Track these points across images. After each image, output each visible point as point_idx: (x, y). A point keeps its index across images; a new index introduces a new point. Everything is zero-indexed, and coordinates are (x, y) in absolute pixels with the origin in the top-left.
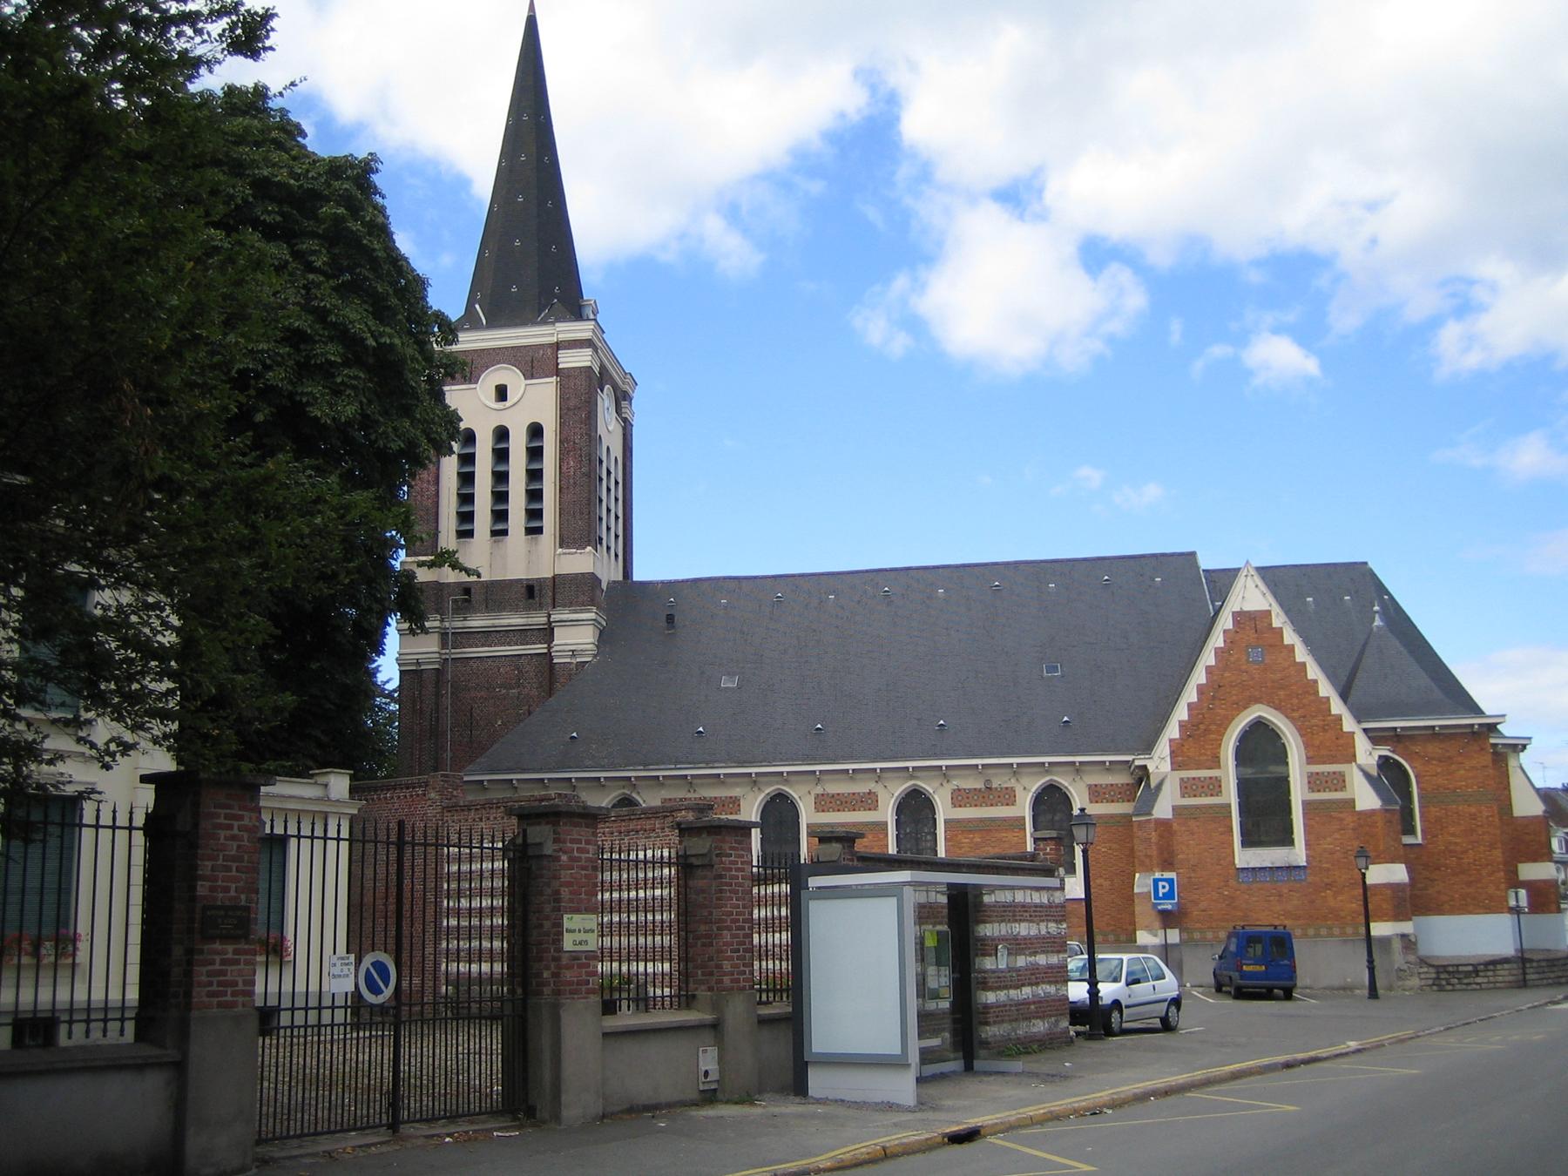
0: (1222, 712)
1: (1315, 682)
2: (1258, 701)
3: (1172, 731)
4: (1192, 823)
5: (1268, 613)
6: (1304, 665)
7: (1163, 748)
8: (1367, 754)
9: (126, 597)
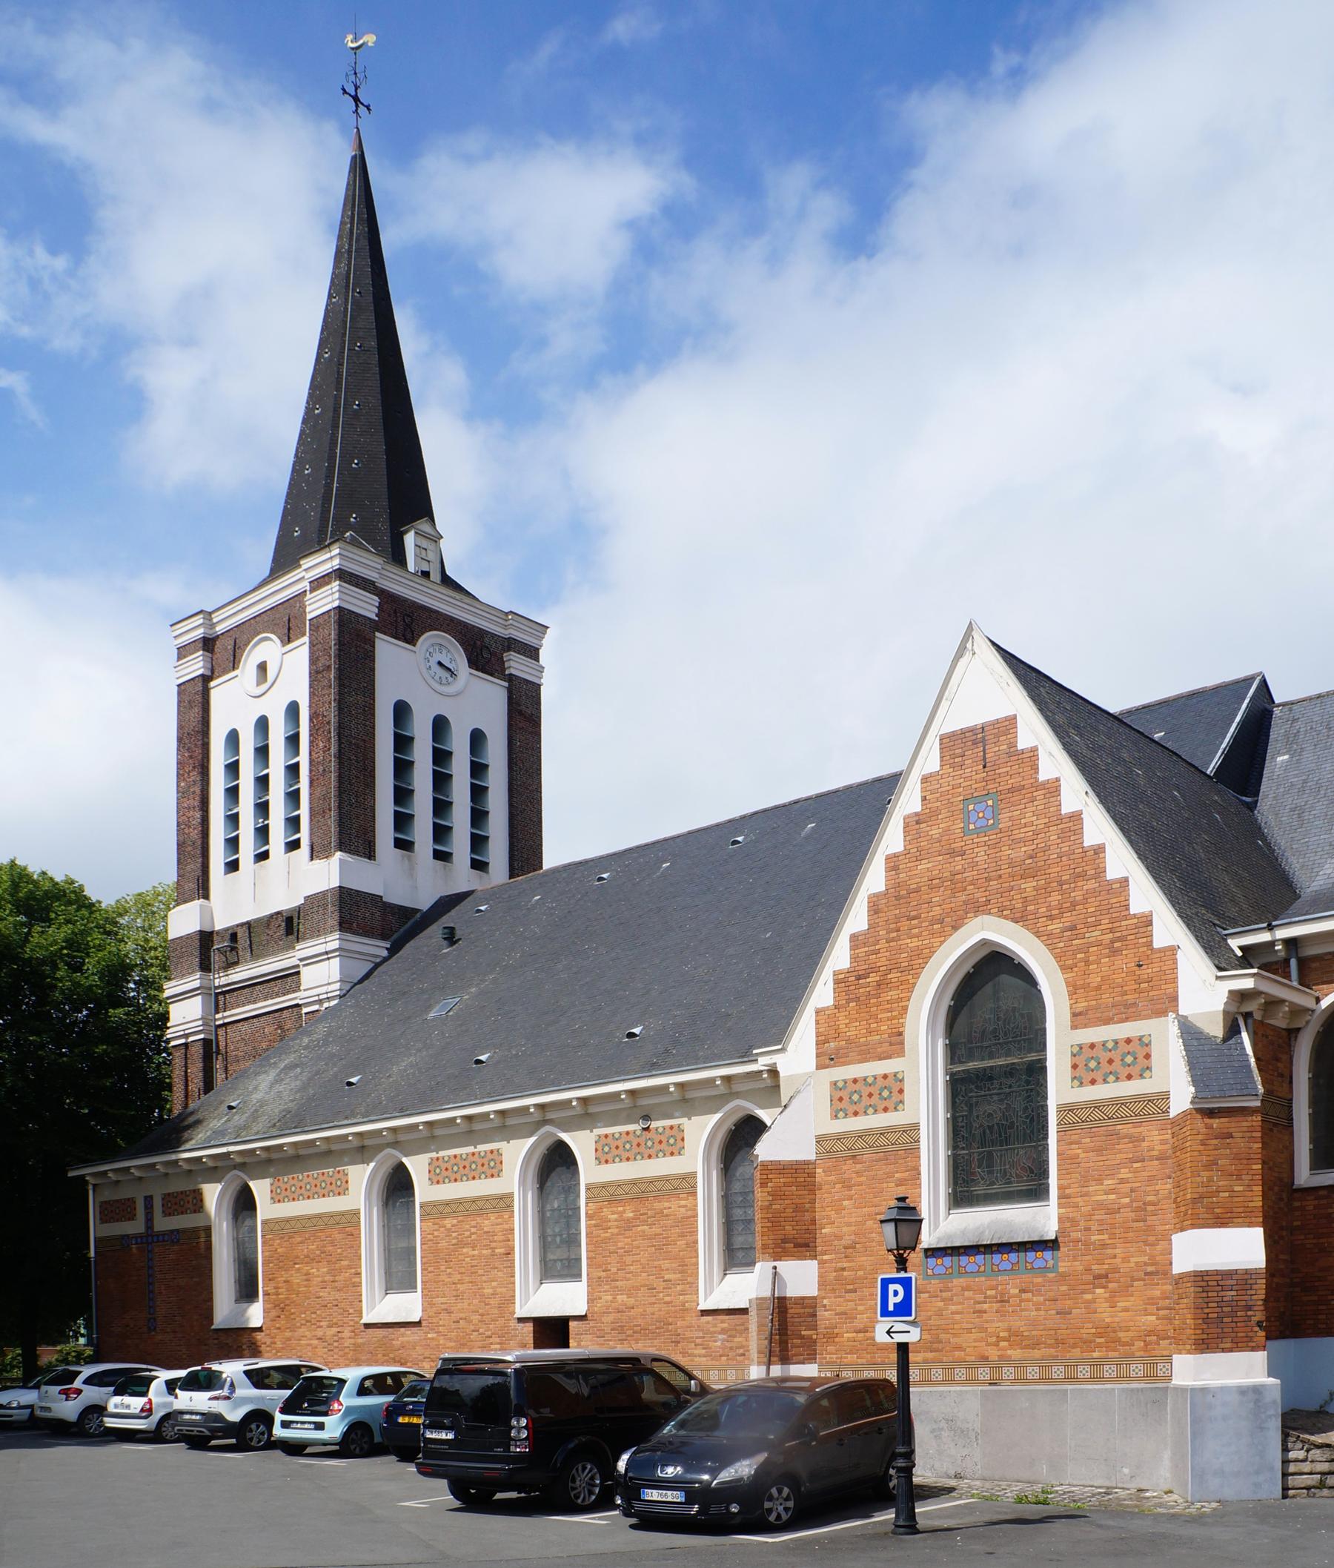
0: (914, 943)
1: (1099, 850)
2: (978, 908)
3: (822, 994)
4: (848, 1167)
5: (1011, 722)
6: (1076, 817)
7: (804, 1033)
8: (1204, 991)
9: (1009, 1352)
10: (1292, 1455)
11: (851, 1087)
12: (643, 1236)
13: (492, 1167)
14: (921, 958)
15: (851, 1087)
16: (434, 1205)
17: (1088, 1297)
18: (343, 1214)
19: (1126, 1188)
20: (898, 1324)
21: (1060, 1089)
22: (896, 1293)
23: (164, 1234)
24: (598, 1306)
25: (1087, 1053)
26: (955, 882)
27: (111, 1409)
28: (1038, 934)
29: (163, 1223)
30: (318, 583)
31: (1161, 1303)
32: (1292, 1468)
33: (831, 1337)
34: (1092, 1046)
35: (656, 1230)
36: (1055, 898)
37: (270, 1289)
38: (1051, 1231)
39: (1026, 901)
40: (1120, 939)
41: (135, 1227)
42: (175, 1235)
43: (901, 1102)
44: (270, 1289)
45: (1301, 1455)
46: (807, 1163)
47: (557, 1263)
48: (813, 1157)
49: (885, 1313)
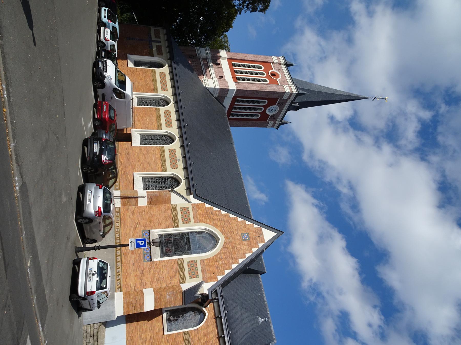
0: (219, 224)
2: (226, 238)
10: (95, 325)
11: (187, 212)
12: (151, 160)
13: (164, 89)
14: (216, 226)
15: (187, 212)
16: (159, 111)
17: (138, 270)
18: (157, 89)
19: (164, 276)
20: (134, 245)
21: (186, 258)
22: (142, 243)
23: (152, 44)
24: (134, 149)
25: (195, 264)
26: (231, 232)
27: (107, 29)
28: (221, 250)
29: (154, 44)
30: (290, 87)
31: (136, 288)
32: (92, 325)
33: (127, 210)
34: (196, 265)
35: (153, 162)
36: (228, 254)
37: (138, 70)
38: (154, 260)
39: (227, 248)
40: (219, 269)
41: (153, 38)
42: (151, 48)
43: (191, 278)
44: (138, 70)
45: (95, 327)
46: (170, 203)
47: (145, 139)
48: (172, 203)
49: (137, 240)
